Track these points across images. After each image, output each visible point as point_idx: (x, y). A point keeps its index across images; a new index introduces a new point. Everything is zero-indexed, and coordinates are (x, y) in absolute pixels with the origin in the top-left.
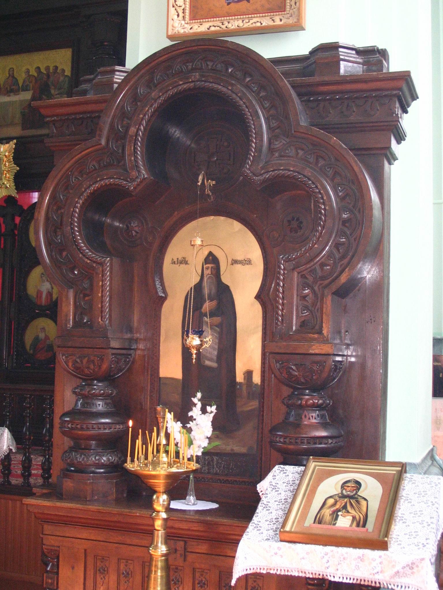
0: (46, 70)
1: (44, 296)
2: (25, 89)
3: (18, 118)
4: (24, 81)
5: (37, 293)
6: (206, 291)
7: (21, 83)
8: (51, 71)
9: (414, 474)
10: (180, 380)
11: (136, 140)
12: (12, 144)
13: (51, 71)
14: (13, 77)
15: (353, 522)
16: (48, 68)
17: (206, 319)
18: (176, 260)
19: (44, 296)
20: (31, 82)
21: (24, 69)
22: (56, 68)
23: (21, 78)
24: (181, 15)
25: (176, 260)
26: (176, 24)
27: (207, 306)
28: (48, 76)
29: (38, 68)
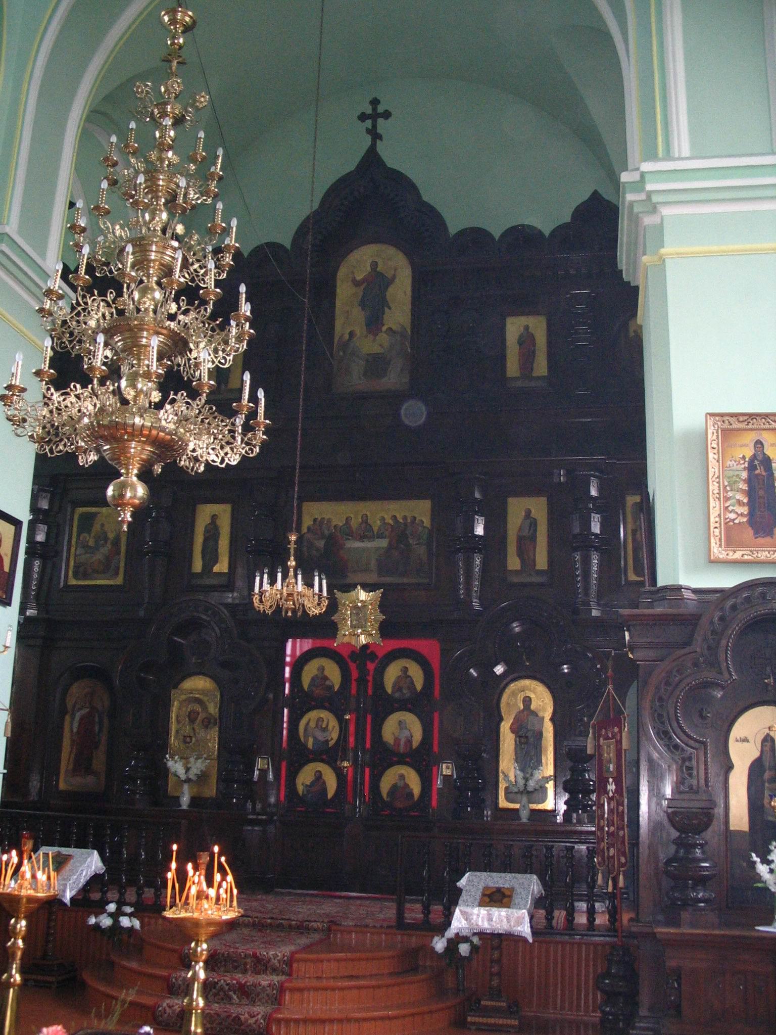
0: (403, 519)
1: (402, 743)
2: (380, 536)
3: (373, 564)
4: (379, 529)
5: (395, 741)
6: (767, 764)
7: (375, 529)
8: (409, 521)
9: (258, 973)
10: (744, 832)
11: (727, 650)
12: (379, 593)
13: (409, 521)
14: (366, 522)
15: (280, 1026)
16: (405, 518)
17: (767, 785)
18: (739, 738)
19: (402, 743)
20: (387, 530)
21: (379, 516)
22: (414, 518)
23: (376, 525)
24: (718, 543)
25: (739, 738)
26: (716, 551)
27: (767, 775)
28: (405, 524)
29: (395, 517)
